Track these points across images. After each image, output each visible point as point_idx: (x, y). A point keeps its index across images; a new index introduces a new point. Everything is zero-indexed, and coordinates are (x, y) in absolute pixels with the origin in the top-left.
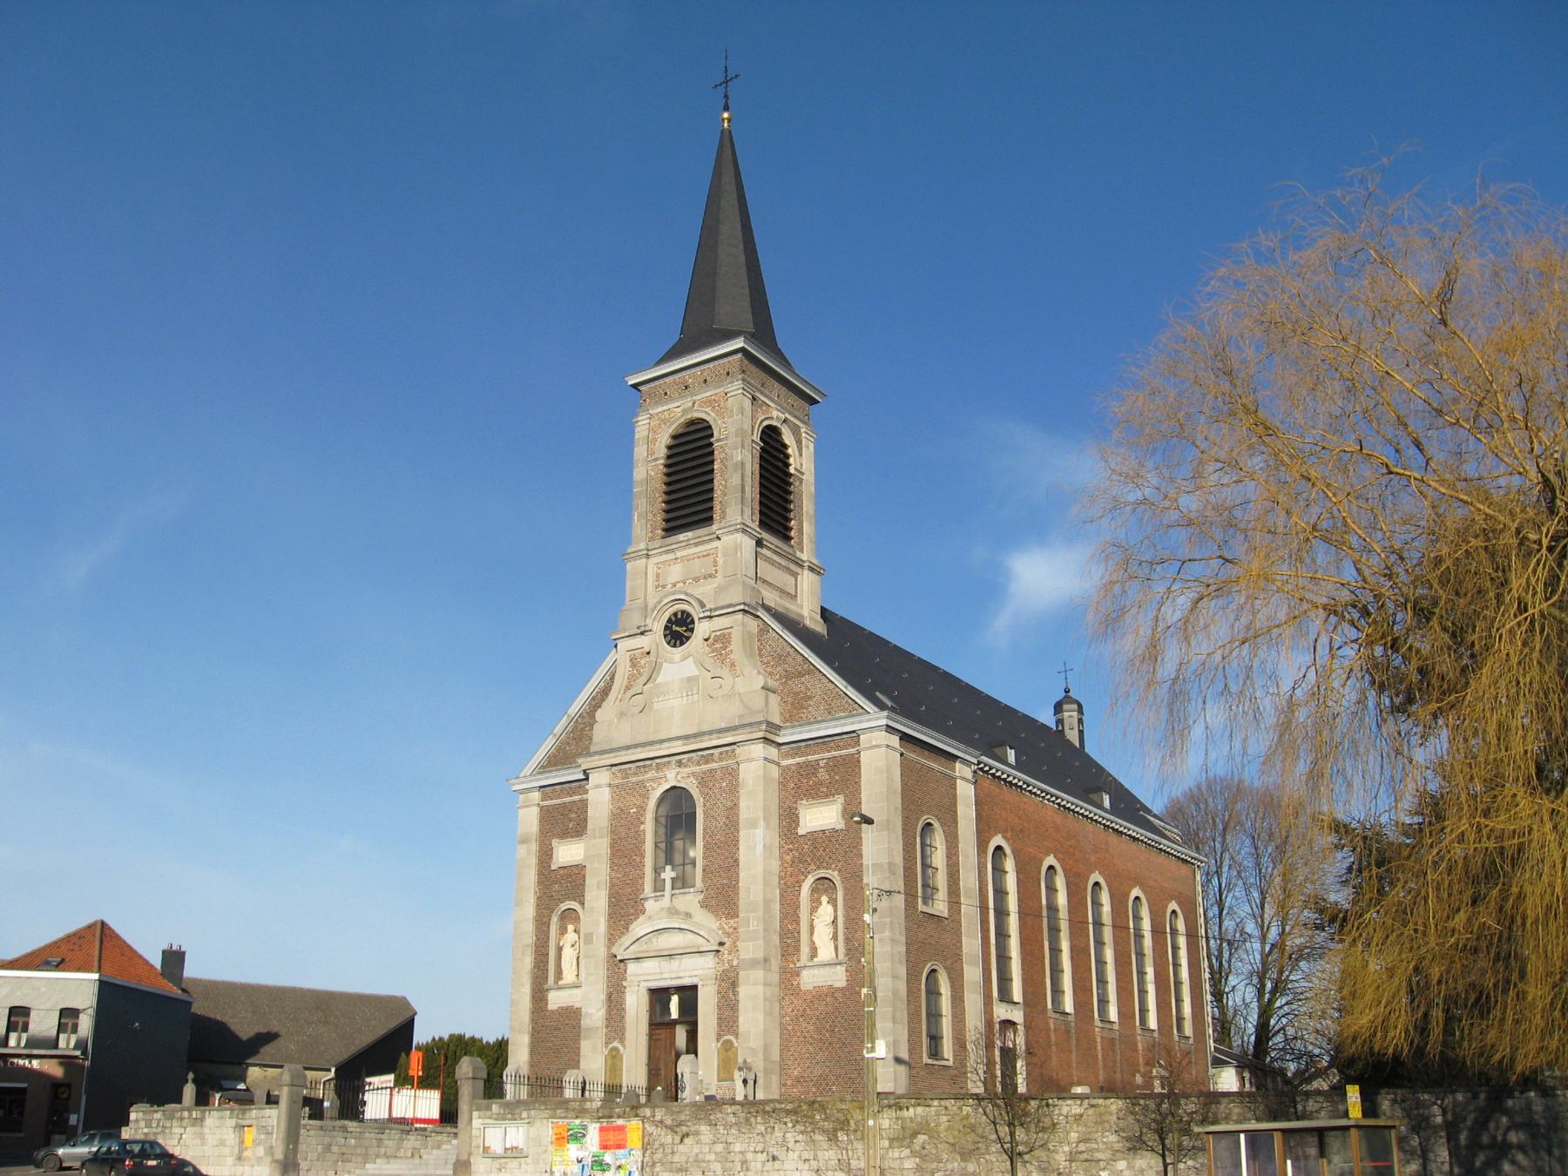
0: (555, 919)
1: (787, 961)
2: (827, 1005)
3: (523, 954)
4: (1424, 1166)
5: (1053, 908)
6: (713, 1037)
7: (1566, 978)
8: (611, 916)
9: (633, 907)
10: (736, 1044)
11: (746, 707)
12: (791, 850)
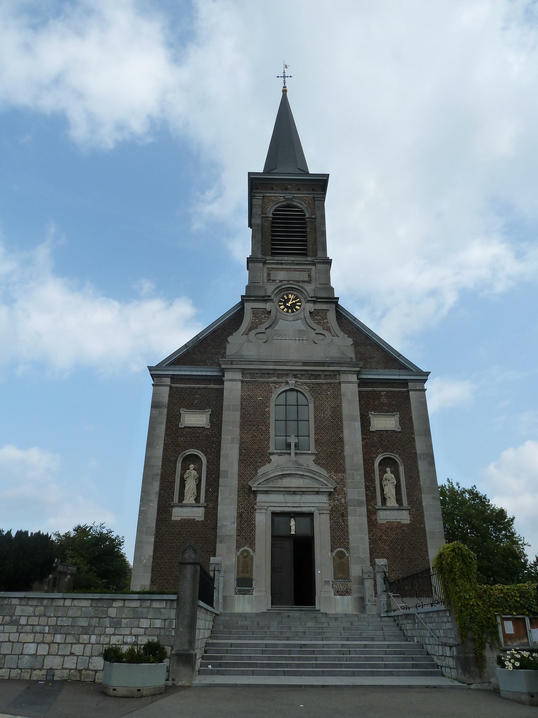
0: (180, 460)
4: (441, 616)
8: (241, 461)
9: (260, 458)
10: (347, 555)
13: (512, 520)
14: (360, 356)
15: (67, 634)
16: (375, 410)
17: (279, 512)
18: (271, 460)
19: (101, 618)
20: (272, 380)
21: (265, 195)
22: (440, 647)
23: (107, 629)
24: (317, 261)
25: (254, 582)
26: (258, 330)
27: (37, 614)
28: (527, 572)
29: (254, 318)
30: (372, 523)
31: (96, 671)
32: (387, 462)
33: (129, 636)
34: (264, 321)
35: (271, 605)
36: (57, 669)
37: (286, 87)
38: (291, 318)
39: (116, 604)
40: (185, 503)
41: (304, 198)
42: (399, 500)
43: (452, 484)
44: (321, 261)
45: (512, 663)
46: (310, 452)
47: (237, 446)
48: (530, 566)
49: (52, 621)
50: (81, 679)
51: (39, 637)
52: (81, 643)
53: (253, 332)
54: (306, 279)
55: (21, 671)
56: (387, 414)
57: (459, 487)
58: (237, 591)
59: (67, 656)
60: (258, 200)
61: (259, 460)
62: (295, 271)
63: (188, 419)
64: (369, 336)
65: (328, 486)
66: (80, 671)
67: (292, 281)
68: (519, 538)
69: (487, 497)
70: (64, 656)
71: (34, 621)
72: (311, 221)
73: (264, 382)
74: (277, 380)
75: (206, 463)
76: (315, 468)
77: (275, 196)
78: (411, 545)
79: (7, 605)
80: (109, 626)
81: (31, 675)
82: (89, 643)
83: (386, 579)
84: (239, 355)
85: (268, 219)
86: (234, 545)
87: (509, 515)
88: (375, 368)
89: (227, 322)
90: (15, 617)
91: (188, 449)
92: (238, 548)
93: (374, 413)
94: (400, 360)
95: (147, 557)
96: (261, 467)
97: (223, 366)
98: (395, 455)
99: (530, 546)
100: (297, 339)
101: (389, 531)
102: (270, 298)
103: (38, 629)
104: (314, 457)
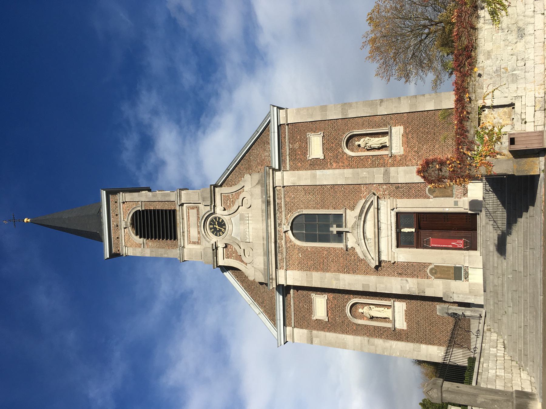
1: (387, 164)
2: (412, 137)
3: (373, 345)
6: (426, 200)
8: (354, 272)
9: (351, 257)
11: (257, 184)
12: (331, 163)
17: (396, 241)
18: (352, 247)
20: (284, 244)
21: (124, 245)
25: (457, 266)
26: (242, 254)
34: (234, 249)
42: (385, 134)
53: (244, 258)
54: (195, 210)
58: (465, 280)
60: (129, 251)
61: (353, 257)
65: (373, 200)
67: (198, 223)
73: (286, 252)
85: (145, 242)
86: (426, 281)
89: (237, 278)
91: (346, 314)
92: (428, 278)
93: (308, 154)
95: (440, 352)
98: (344, 137)
100: (247, 219)
101: (410, 145)
104: (348, 211)
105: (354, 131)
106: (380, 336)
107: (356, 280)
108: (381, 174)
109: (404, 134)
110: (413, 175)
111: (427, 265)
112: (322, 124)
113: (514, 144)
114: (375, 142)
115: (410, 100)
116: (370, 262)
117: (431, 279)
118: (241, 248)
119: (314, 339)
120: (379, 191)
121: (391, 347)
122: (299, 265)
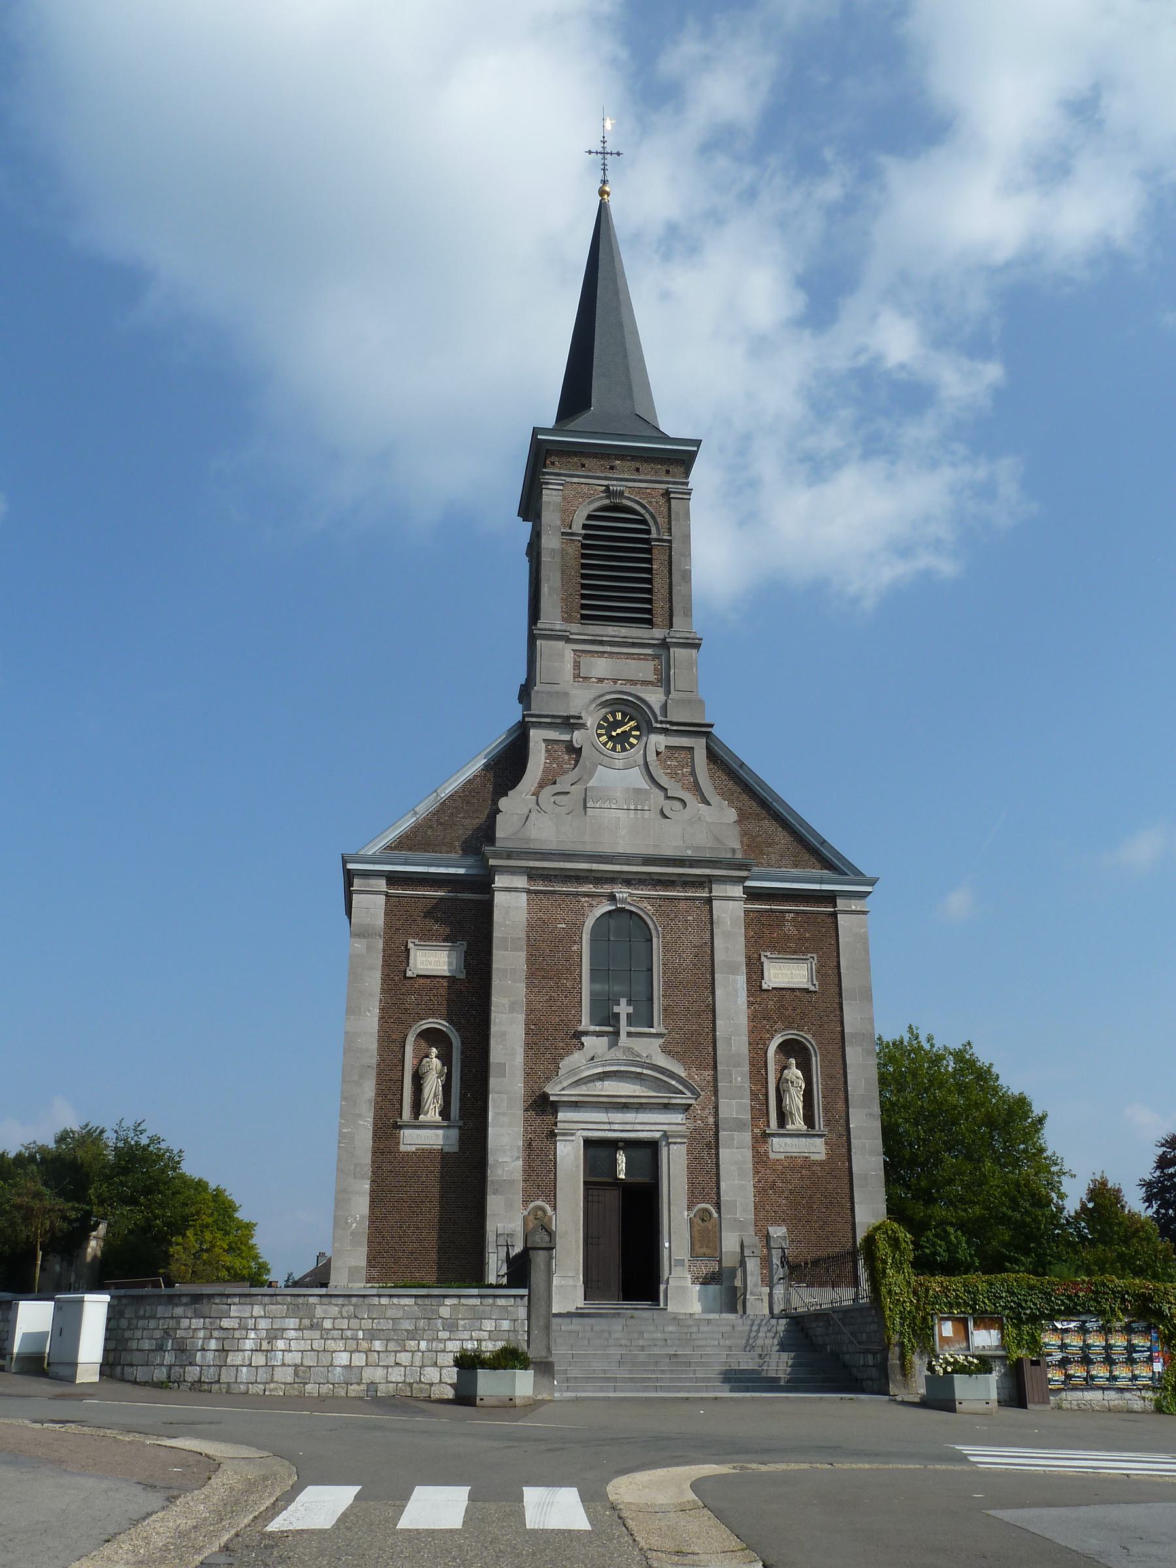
5: (816, 1057)
6: (685, 1204)
7: (1064, 1160)
8: (529, 1046)
13: (1041, 1120)
14: (753, 844)
15: (388, 1340)
16: (773, 949)
18: (583, 1044)
19: (430, 1319)
20: (586, 890)
22: (862, 1356)
23: (440, 1333)
24: (674, 640)
26: (558, 788)
27: (345, 1314)
28: (1060, 1232)
29: (548, 761)
30: (760, 1159)
31: (431, 1384)
32: (791, 1048)
33: (470, 1342)
35: (585, 1300)
36: (380, 1383)
37: (607, 181)
38: (619, 764)
39: (448, 1302)
40: (423, 1120)
41: (649, 491)
42: (809, 1119)
43: (918, 1037)
44: (681, 641)
45: (943, 1368)
46: (653, 1031)
47: (521, 1017)
48: (1067, 1220)
49: (367, 1324)
50: (412, 1394)
51: (352, 1344)
52: (407, 1351)
53: (548, 791)
55: (333, 1387)
56: (794, 957)
57: (932, 1046)
59: (391, 1366)
60: (554, 492)
61: (561, 1044)
62: (627, 658)
63: (423, 959)
64: (767, 799)
65: (685, 1094)
66: (411, 1385)
67: (622, 680)
68: (1053, 1158)
69: (994, 1070)
70: (387, 1367)
71: (344, 1324)
72: (661, 546)
74: (594, 890)
75: (460, 1045)
76: (662, 1061)
77: (588, 484)
78: (826, 1197)
79: (302, 1304)
80: (442, 1329)
81: (347, 1391)
82: (419, 1351)
83: (785, 1260)
84: (522, 839)
86: (519, 1197)
87: (1037, 1111)
88: (776, 866)
90: (317, 1320)
91: (424, 1019)
92: (526, 1202)
94: (824, 851)
95: (358, 1219)
96: (565, 1058)
97: (492, 862)
98: (805, 1035)
99: (1075, 1176)
100: (632, 807)
102: (581, 720)
103: (349, 1333)
105: (818, 1058)
106: (381, 1093)
107: (514, 1048)
108: (737, 1114)
109: (810, 1161)
110: (736, 1178)
111: (552, 1201)
112: (834, 989)
113: (1032, 1365)
114: (795, 1101)
115: (876, 1174)
116: (557, 1083)
117: (522, 1207)
118: (571, 785)
119: (364, 941)
120: (703, 1109)
121: (360, 1116)
122: (539, 923)
